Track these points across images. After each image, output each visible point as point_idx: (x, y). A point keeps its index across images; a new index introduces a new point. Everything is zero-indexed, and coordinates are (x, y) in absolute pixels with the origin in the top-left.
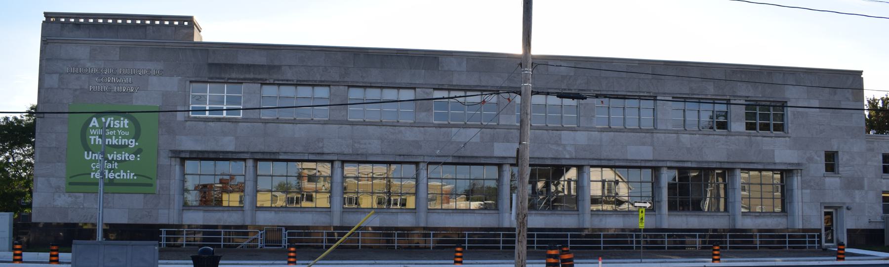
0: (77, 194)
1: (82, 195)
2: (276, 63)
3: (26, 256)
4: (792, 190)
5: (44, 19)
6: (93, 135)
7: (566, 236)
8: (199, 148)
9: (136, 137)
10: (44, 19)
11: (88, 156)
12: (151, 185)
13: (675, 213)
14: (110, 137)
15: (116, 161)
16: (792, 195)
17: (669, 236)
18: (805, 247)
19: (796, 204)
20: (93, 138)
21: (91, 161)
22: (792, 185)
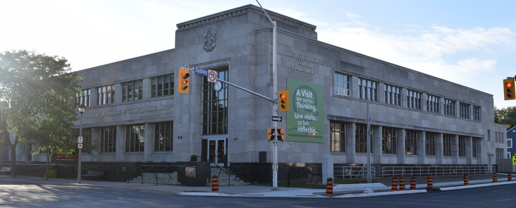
0: (291, 142)
1: (293, 143)
2: (363, 66)
3: (48, 179)
4: (480, 147)
5: (177, 29)
6: (298, 101)
7: (401, 169)
8: (339, 115)
9: (316, 105)
10: (177, 29)
11: (297, 116)
12: (321, 137)
13: (363, 154)
14: (305, 103)
15: (308, 120)
16: (480, 149)
17: (395, 169)
18: (442, 175)
19: (482, 153)
20: (298, 103)
21: (298, 119)
22: (480, 145)
